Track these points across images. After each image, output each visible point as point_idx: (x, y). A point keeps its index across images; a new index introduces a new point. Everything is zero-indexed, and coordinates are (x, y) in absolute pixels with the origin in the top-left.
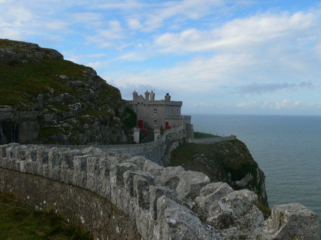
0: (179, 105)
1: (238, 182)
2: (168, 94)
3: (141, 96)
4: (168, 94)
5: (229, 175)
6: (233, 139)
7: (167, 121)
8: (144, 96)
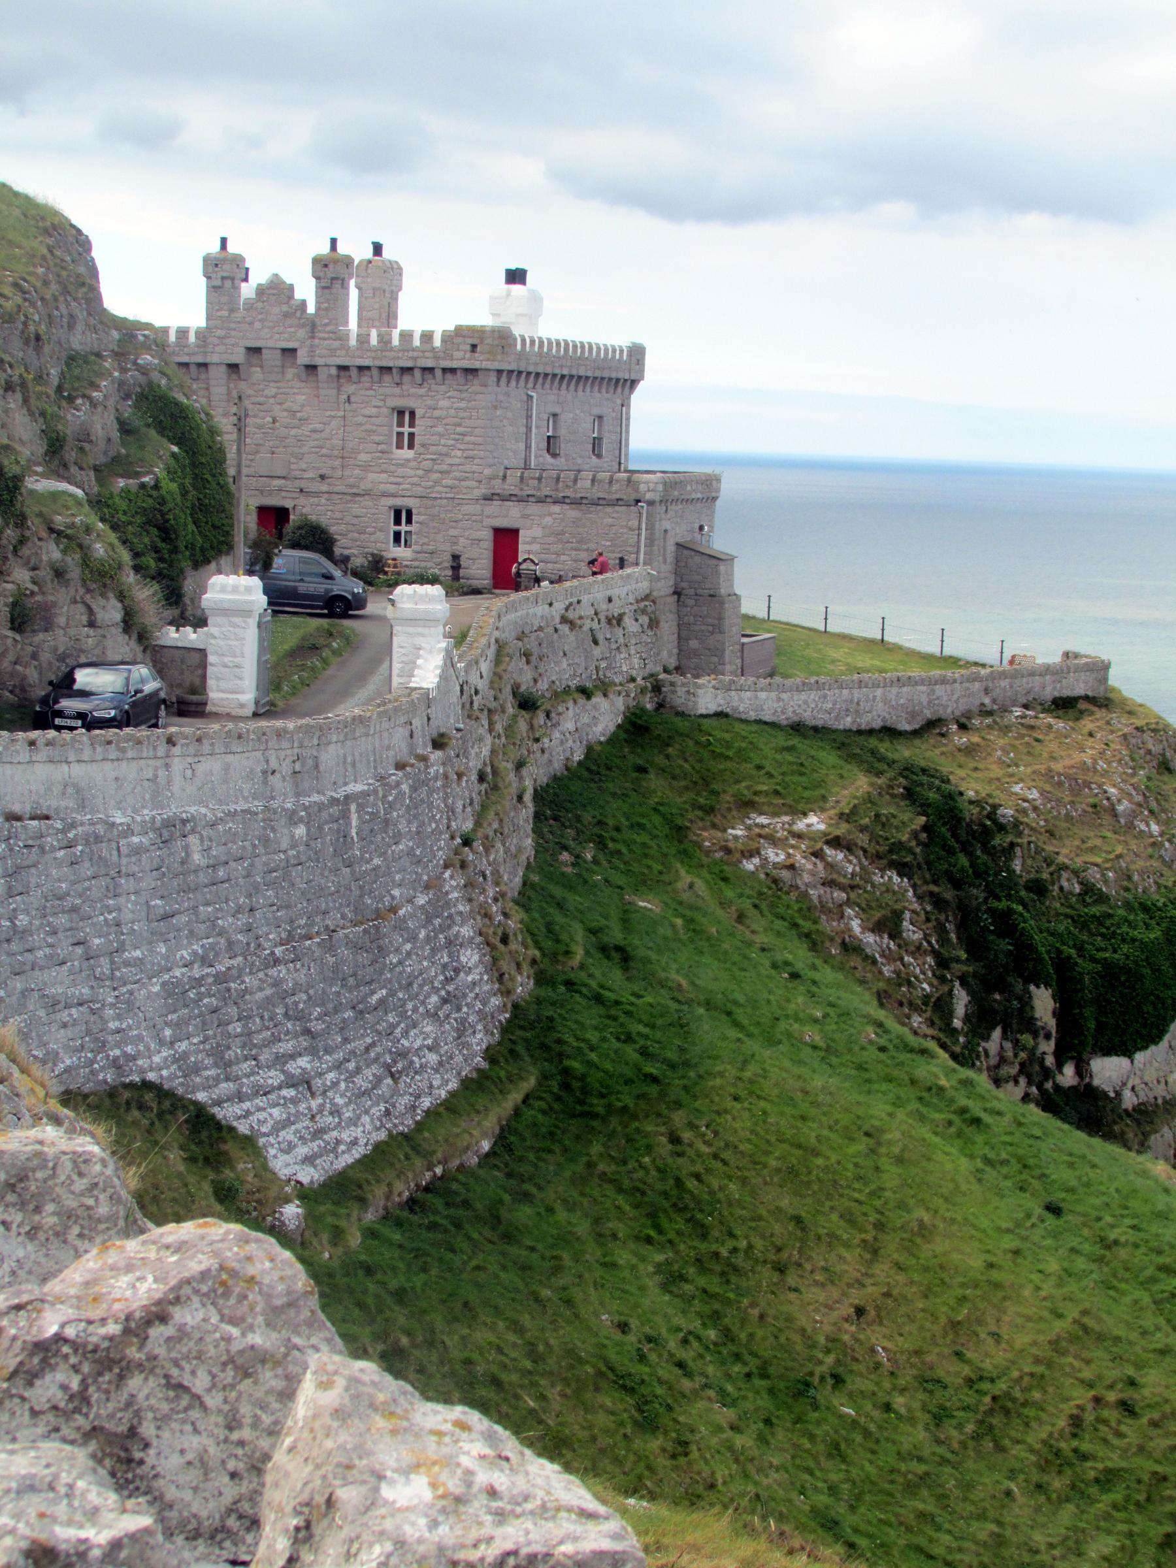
1: (1108, 1070)
3: (277, 290)
5: (1043, 1003)
6: (1078, 687)
7: (510, 515)
8: (306, 291)
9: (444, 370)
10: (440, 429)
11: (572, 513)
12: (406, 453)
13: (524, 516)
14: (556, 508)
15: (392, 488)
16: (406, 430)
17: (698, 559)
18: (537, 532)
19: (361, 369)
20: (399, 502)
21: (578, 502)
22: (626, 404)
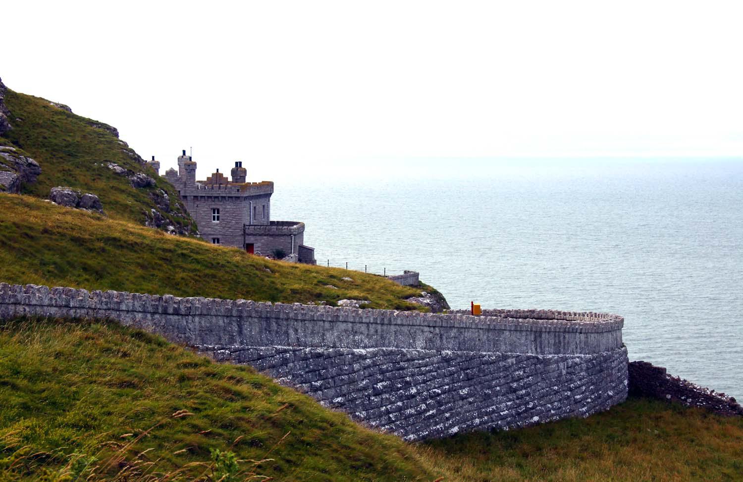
0: (265, 190)
2: (238, 164)
4: (238, 164)
9: (229, 197)
10: (227, 215)
11: (271, 239)
12: (216, 222)
13: (256, 240)
14: (265, 237)
15: (212, 233)
16: (216, 215)
17: (305, 250)
18: (259, 244)
19: (201, 197)
20: (215, 237)
21: (271, 236)
22: (269, 201)
